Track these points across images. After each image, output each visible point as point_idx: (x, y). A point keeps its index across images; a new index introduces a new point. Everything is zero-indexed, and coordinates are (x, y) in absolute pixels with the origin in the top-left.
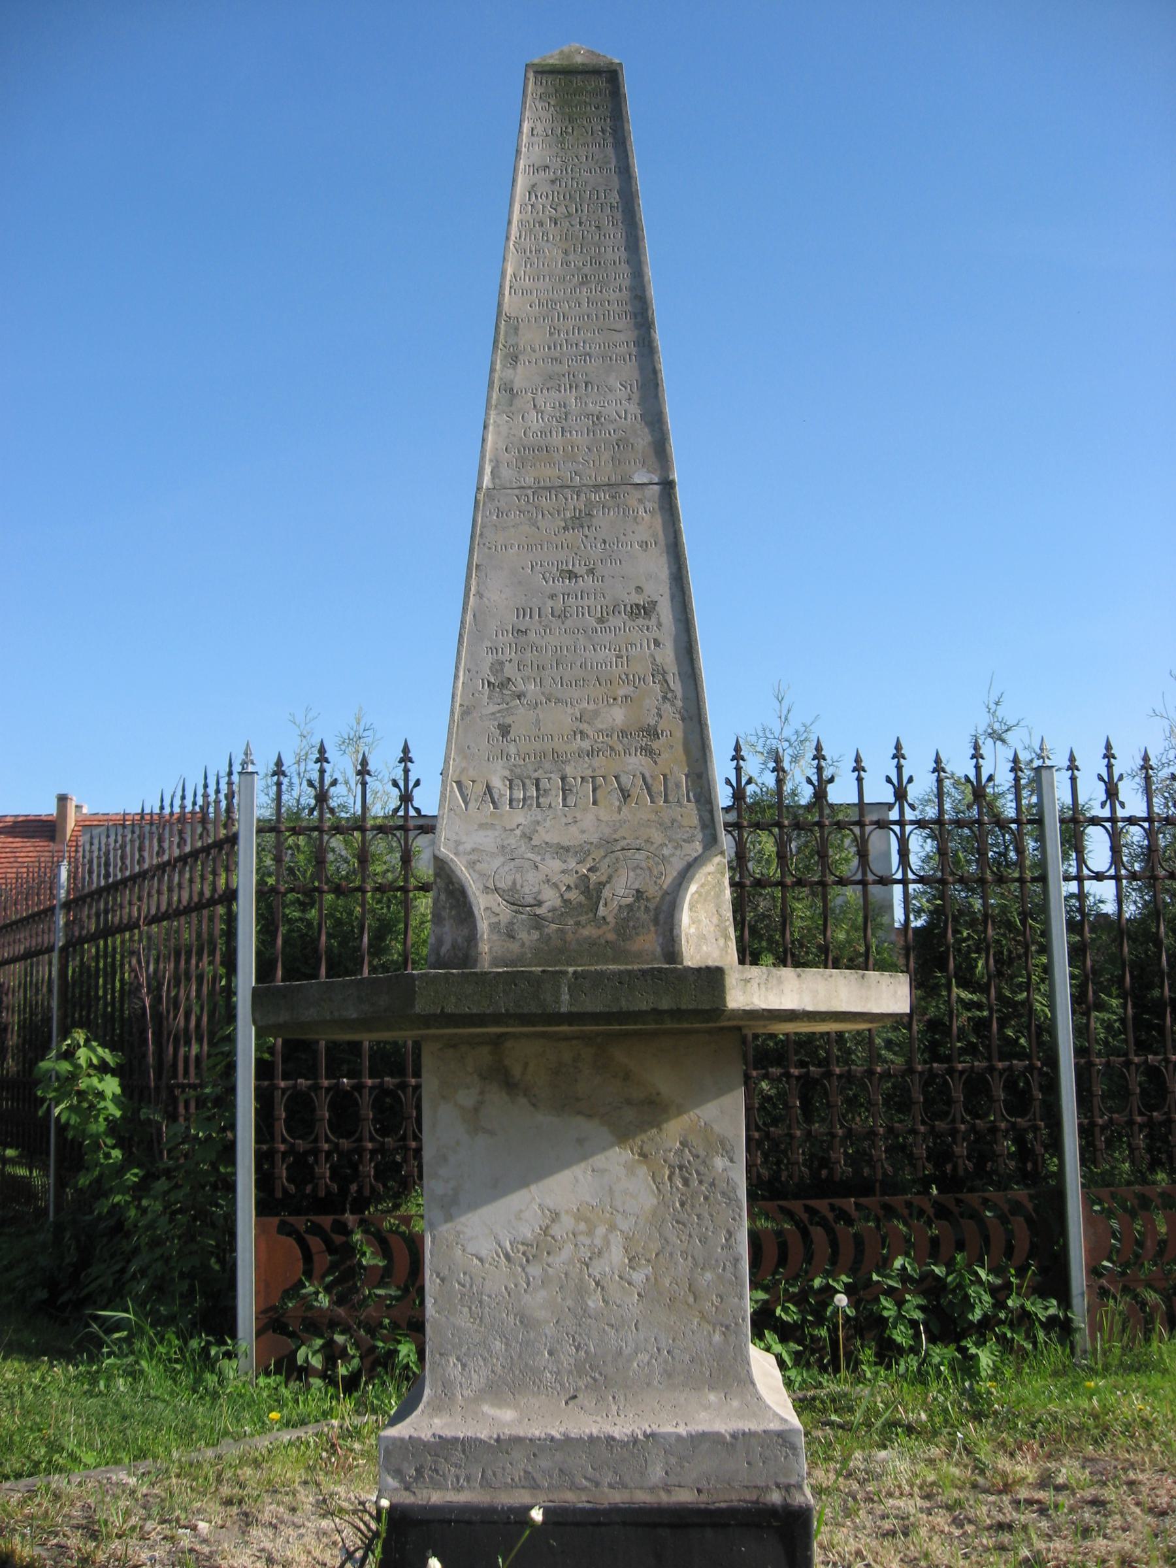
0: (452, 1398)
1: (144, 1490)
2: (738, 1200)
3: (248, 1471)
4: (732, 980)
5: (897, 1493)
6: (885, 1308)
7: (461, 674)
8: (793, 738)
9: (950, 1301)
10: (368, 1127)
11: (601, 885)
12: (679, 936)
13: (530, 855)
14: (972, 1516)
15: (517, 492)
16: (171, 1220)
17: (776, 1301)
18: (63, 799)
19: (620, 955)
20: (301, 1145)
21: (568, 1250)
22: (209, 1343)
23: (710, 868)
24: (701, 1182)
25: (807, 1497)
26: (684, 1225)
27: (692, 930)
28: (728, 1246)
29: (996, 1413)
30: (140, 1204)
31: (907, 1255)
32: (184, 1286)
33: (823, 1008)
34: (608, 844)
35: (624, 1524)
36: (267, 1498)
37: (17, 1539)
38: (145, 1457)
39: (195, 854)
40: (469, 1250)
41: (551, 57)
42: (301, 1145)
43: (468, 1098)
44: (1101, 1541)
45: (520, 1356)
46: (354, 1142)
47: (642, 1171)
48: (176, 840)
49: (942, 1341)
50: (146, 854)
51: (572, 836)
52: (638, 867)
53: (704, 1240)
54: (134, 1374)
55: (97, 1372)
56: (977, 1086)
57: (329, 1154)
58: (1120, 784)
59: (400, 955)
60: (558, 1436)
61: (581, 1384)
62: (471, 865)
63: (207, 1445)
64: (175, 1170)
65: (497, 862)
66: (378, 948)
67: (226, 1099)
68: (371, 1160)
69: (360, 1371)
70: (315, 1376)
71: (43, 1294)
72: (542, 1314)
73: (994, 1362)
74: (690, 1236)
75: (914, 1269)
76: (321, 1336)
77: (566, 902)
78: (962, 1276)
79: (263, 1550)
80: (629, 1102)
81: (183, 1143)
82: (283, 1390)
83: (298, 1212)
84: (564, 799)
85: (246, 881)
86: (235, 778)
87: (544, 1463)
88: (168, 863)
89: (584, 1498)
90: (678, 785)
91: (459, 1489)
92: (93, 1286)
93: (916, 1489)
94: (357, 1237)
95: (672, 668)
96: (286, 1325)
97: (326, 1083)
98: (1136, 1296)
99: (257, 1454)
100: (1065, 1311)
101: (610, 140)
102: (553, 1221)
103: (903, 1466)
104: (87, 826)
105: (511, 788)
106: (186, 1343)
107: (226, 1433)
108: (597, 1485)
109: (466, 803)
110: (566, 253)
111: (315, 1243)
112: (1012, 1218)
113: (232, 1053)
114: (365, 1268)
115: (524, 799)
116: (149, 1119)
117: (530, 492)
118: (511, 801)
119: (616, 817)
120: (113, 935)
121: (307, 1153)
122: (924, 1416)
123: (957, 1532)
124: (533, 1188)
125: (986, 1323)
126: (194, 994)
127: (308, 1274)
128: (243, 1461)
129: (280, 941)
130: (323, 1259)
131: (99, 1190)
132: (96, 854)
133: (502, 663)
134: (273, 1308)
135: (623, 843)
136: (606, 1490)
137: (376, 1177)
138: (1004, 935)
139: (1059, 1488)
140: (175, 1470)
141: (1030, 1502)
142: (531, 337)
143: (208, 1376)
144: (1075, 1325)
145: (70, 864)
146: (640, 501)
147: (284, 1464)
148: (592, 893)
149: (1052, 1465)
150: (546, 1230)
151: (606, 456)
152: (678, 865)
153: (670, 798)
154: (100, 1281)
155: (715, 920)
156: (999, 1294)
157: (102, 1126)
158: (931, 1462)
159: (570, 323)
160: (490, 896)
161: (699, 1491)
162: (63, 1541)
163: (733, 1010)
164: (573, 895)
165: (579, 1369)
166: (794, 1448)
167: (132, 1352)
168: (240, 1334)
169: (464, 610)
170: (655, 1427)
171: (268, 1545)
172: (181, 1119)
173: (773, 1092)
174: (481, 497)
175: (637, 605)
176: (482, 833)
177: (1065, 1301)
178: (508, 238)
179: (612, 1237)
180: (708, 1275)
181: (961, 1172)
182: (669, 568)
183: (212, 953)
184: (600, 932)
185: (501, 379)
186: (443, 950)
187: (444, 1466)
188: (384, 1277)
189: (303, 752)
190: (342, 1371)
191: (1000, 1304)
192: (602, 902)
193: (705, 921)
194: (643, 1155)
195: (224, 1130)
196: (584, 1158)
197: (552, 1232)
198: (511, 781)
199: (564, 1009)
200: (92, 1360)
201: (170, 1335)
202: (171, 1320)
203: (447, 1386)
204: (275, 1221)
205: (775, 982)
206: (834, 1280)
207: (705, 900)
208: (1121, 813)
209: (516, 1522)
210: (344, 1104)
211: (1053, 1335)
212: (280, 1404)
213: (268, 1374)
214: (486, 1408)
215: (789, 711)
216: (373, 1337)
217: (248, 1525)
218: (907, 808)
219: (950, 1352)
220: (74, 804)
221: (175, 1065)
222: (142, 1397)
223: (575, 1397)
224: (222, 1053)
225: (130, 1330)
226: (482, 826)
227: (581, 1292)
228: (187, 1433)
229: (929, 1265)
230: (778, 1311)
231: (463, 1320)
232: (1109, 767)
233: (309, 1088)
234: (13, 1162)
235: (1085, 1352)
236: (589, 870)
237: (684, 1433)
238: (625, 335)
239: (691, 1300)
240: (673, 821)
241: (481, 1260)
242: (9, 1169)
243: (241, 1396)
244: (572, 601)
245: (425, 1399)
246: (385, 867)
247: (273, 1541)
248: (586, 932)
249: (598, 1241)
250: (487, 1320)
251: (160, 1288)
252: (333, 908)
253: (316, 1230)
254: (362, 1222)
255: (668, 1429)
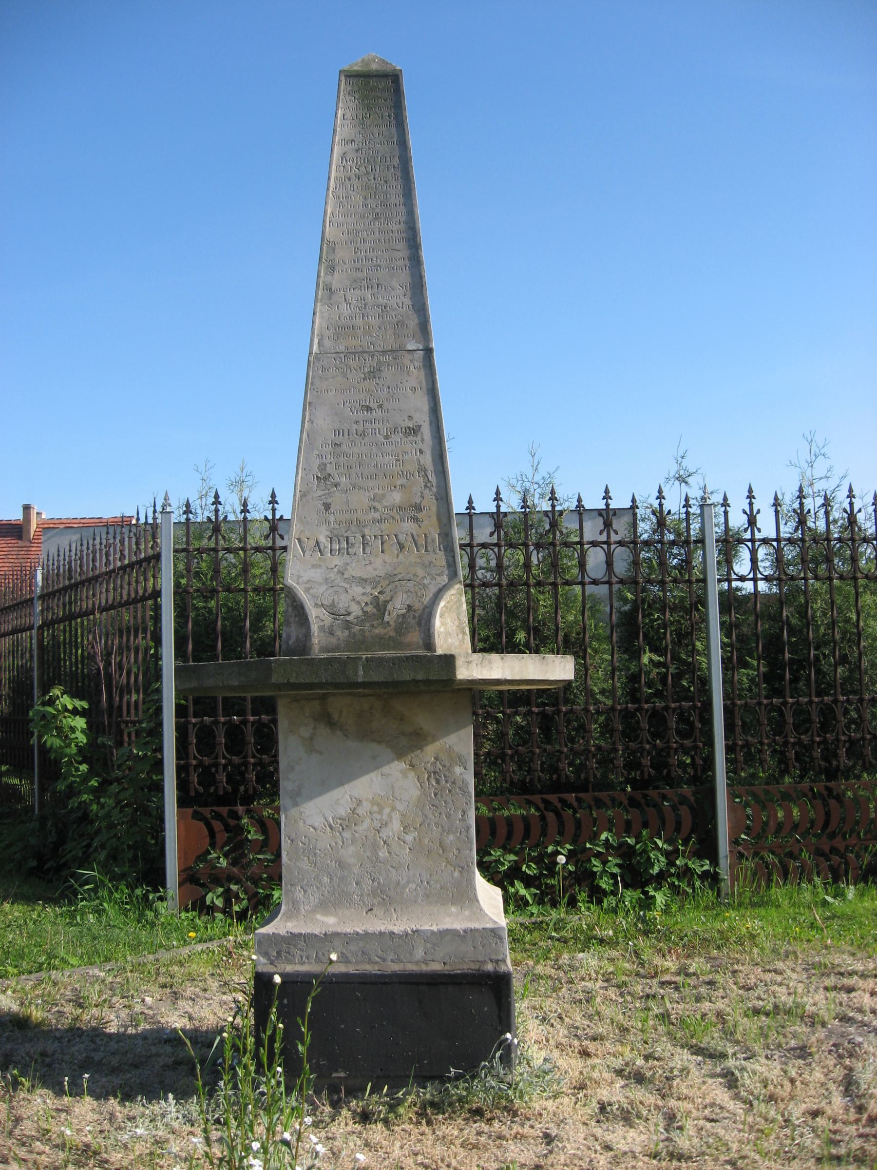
0: (298, 910)
1: (110, 979)
2: (469, 793)
3: (176, 968)
4: (459, 663)
5: (587, 979)
6: (594, 866)
7: (300, 472)
8: (541, 482)
9: (638, 862)
10: (251, 749)
11: (387, 602)
12: (434, 633)
13: (342, 584)
14: (632, 991)
15: (334, 355)
16: (121, 812)
17: (523, 861)
18: (27, 508)
19: (399, 645)
20: (207, 760)
21: (368, 821)
22: (148, 891)
23: (453, 591)
24: (447, 782)
25: (509, 966)
26: (437, 807)
27: (442, 629)
28: (463, 820)
29: (659, 931)
30: (99, 800)
31: (610, 831)
32: (130, 855)
33: (517, 678)
34: (391, 577)
35: (400, 983)
36: (188, 984)
37: (33, 1007)
38: (110, 960)
39: (131, 565)
40: (308, 822)
41: (357, 64)
42: (207, 760)
43: (306, 732)
44: (708, 1004)
45: (339, 886)
46: (243, 758)
47: (412, 775)
48: (118, 556)
49: (632, 888)
50: (98, 564)
51: (368, 572)
52: (409, 591)
53: (448, 816)
54: (99, 912)
55: (75, 911)
56: (657, 717)
57: (225, 767)
58: (758, 516)
59: (272, 631)
60: (361, 932)
61: (375, 902)
62: (307, 590)
63: (149, 953)
64: (122, 778)
65: (323, 588)
66: (256, 627)
67: (156, 731)
68: (253, 770)
69: (248, 908)
70: (218, 912)
71: (33, 863)
72: (351, 861)
73: (666, 901)
74: (440, 814)
75: (613, 840)
76: (222, 886)
77: (365, 613)
78: (646, 844)
79: (186, 1012)
80: (403, 734)
81: (127, 760)
82: (197, 920)
83: (206, 805)
84: (364, 549)
85: (167, 583)
86: (158, 515)
87: (353, 948)
88: (113, 571)
89: (377, 968)
90: (433, 541)
91: (303, 963)
92: (69, 856)
93: (600, 976)
94: (245, 821)
95: (430, 467)
96: (199, 879)
97: (222, 719)
98: (762, 858)
99: (181, 958)
100: (715, 868)
101: (394, 122)
102: (358, 805)
103: (594, 963)
104: (48, 528)
105: (331, 543)
106: (133, 891)
107: (161, 946)
108: (384, 960)
109: (304, 553)
110: (365, 198)
111: (217, 825)
112: (680, 807)
113: (160, 700)
114: (250, 841)
115: (339, 550)
116: (104, 744)
117: (342, 355)
118: (331, 551)
119: (395, 560)
120: (76, 618)
121: (210, 766)
122: (611, 933)
123: (621, 1000)
124: (346, 786)
125: (662, 876)
126: (132, 660)
127: (213, 845)
128: (172, 962)
129: (190, 625)
130: (222, 836)
131: (72, 792)
132: (62, 562)
133: (325, 465)
134: (190, 868)
135: (400, 577)
136: (389, 963)
137: (258, 782)
138: (682, 617)
139: (687, 975)
140: (129, 968)
141: (670, 983)
142: (343, 254)
143: (147, 912)
144: (721, 877)
145: (43, 569)
146: (411, 361)
147: (198, 965)
148: (381, 607)
149: (688, 962)
150: (353, 811)
151: (390, 332)
152: (433, 589)
153: (429, 549)
154: (73, 853)
155: (456, 623)
156: (671, 857)
157: (73, 750)
158: (611, 960)
159: (368, 245)
160: (318, 610)
161: (445, 964)
162: (62, 1009)
163: (460, 680)
164: (369, 609)
165: (374, 893)
166: (501, 938)
167: (98, 898)
168: (169, 885)
169: (302, 432)
170: (418, 927)
171: (190, 1010)
172: (126, 744)
173: (523, 724)
174: (312, 359)
175: (409, 428)
176: (313, 570)
177: (715, 861)
178: (328, 189)
179: (393, 814)
180: (451, 837)
181: (646, 777)
182: (429, 404)
183: (145, 631)
184: (386, 631)
185: (324, 282)
186: (291, 642)
187: (293, 950)
188: (263, 846)
189: (204, 493)
190: (236, 908)
191: (671, 863)
192: (387, 613)
193: (450, 624)
194: (412, 766)
195: (155, 751)
196: (377, 768)
197: (357, 811)
198: (331, 538)
199: (360, 680)
200: (70, 904)
201: (122, 887)
202: (123, 876)
203: (295, 903)
204: (190, 811)
205: (487, 662)
206: (561, 848)
207: (450, 611)
208: (758, 536)
209: (336, 983)
210: (235, 734)
211: (706, 883)
212: (195, 929)
213: (187, 911)
214: (318, 917)
215: (538, 463)
216: (257, 887)
217: (176, 999)
218: (612, 533)
219: (637, 894)
220: (35, 511)
221: (120, 707)
222: (105, 926)
223: (372, 909)
224: (152, 700)
225: (96, 884)
226: (314, 566)
227: (375, 847)
228: (135, 947)
229: (624, 837)
230: (524, 868)
231: (304, 864)
232: (751, 504)
233: (212, 722)
234: (8, 773)
235: (727, 894)
236: (379, 593)
237: (436, 930)
238: (403, 252)
239: (441, 852)
240: (430, 563)
241: (315, 829)
242: (4, 779)
243: (169, 924)
244: (368, 425)
245: (282, 911)
246: (262, 571)
247: (193, 1007)
248: (377, 631)
249: (385, 817)
250: (319, 864)
251: (114, 857)
252: (227, 599)
253: (218, 816)
254: (248, 811)
255: (426, 927)
